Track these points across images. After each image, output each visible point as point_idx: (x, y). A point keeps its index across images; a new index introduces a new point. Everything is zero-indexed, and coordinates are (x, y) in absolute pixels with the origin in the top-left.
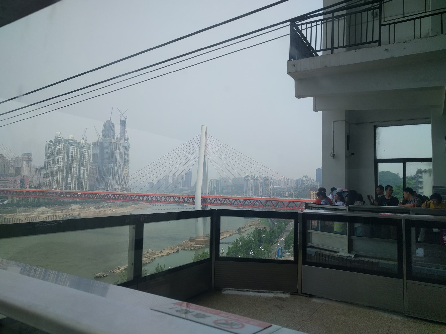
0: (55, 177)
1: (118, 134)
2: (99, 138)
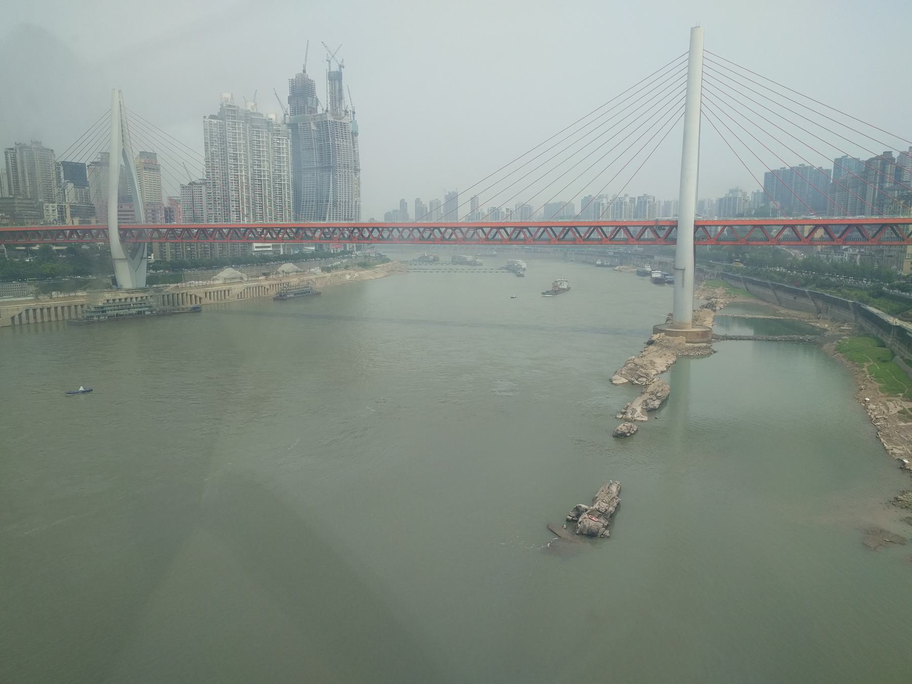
0: (232, 201)
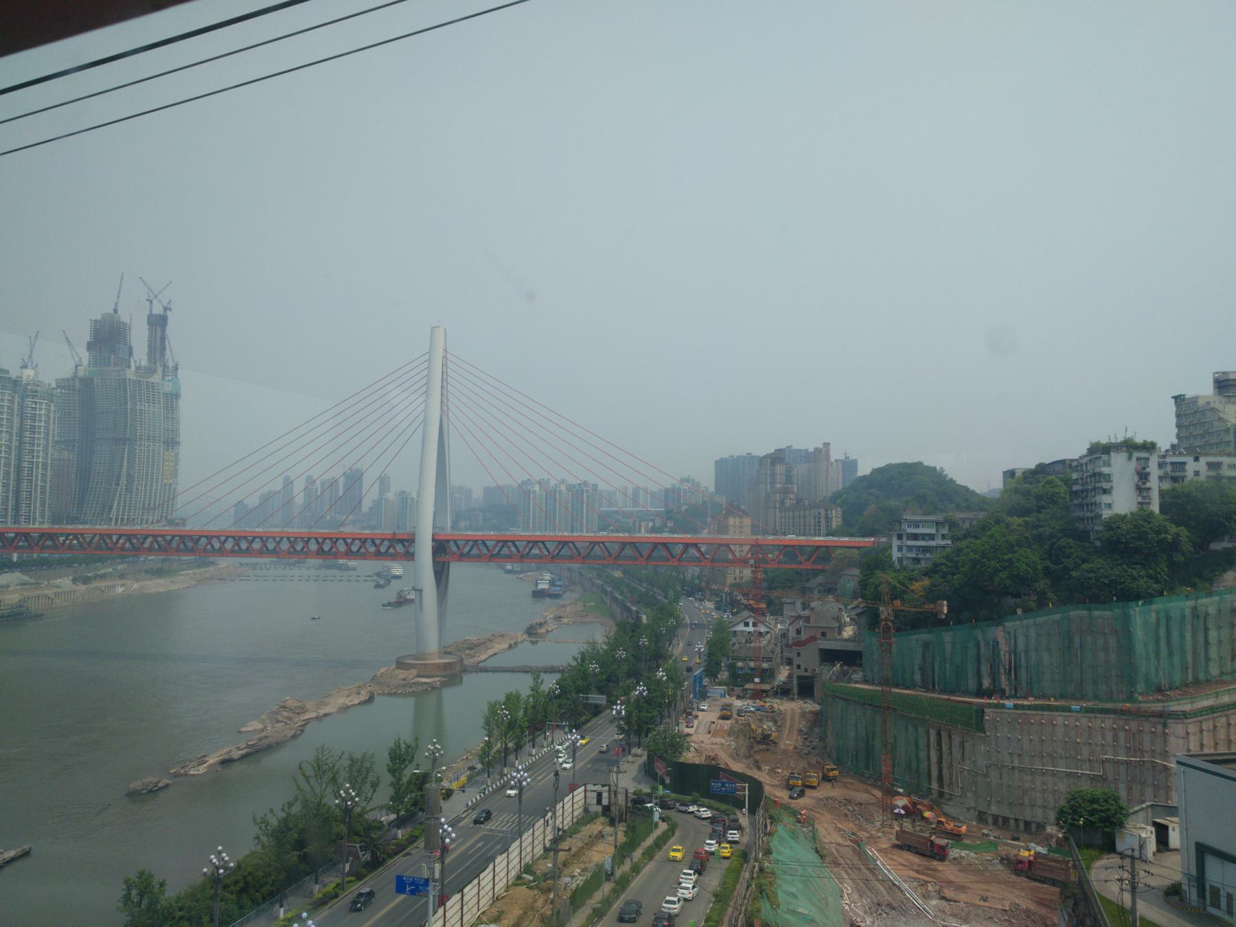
1: (140, 354)
2: (79, 368)
